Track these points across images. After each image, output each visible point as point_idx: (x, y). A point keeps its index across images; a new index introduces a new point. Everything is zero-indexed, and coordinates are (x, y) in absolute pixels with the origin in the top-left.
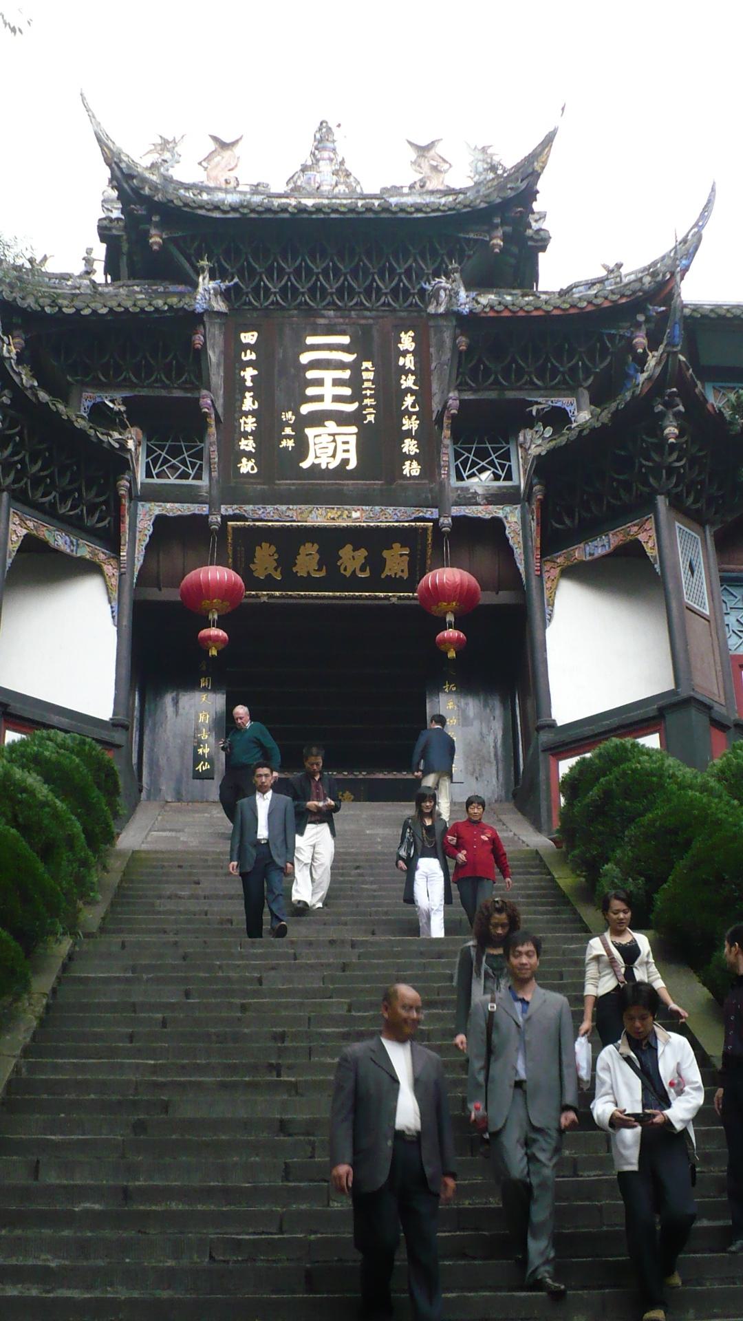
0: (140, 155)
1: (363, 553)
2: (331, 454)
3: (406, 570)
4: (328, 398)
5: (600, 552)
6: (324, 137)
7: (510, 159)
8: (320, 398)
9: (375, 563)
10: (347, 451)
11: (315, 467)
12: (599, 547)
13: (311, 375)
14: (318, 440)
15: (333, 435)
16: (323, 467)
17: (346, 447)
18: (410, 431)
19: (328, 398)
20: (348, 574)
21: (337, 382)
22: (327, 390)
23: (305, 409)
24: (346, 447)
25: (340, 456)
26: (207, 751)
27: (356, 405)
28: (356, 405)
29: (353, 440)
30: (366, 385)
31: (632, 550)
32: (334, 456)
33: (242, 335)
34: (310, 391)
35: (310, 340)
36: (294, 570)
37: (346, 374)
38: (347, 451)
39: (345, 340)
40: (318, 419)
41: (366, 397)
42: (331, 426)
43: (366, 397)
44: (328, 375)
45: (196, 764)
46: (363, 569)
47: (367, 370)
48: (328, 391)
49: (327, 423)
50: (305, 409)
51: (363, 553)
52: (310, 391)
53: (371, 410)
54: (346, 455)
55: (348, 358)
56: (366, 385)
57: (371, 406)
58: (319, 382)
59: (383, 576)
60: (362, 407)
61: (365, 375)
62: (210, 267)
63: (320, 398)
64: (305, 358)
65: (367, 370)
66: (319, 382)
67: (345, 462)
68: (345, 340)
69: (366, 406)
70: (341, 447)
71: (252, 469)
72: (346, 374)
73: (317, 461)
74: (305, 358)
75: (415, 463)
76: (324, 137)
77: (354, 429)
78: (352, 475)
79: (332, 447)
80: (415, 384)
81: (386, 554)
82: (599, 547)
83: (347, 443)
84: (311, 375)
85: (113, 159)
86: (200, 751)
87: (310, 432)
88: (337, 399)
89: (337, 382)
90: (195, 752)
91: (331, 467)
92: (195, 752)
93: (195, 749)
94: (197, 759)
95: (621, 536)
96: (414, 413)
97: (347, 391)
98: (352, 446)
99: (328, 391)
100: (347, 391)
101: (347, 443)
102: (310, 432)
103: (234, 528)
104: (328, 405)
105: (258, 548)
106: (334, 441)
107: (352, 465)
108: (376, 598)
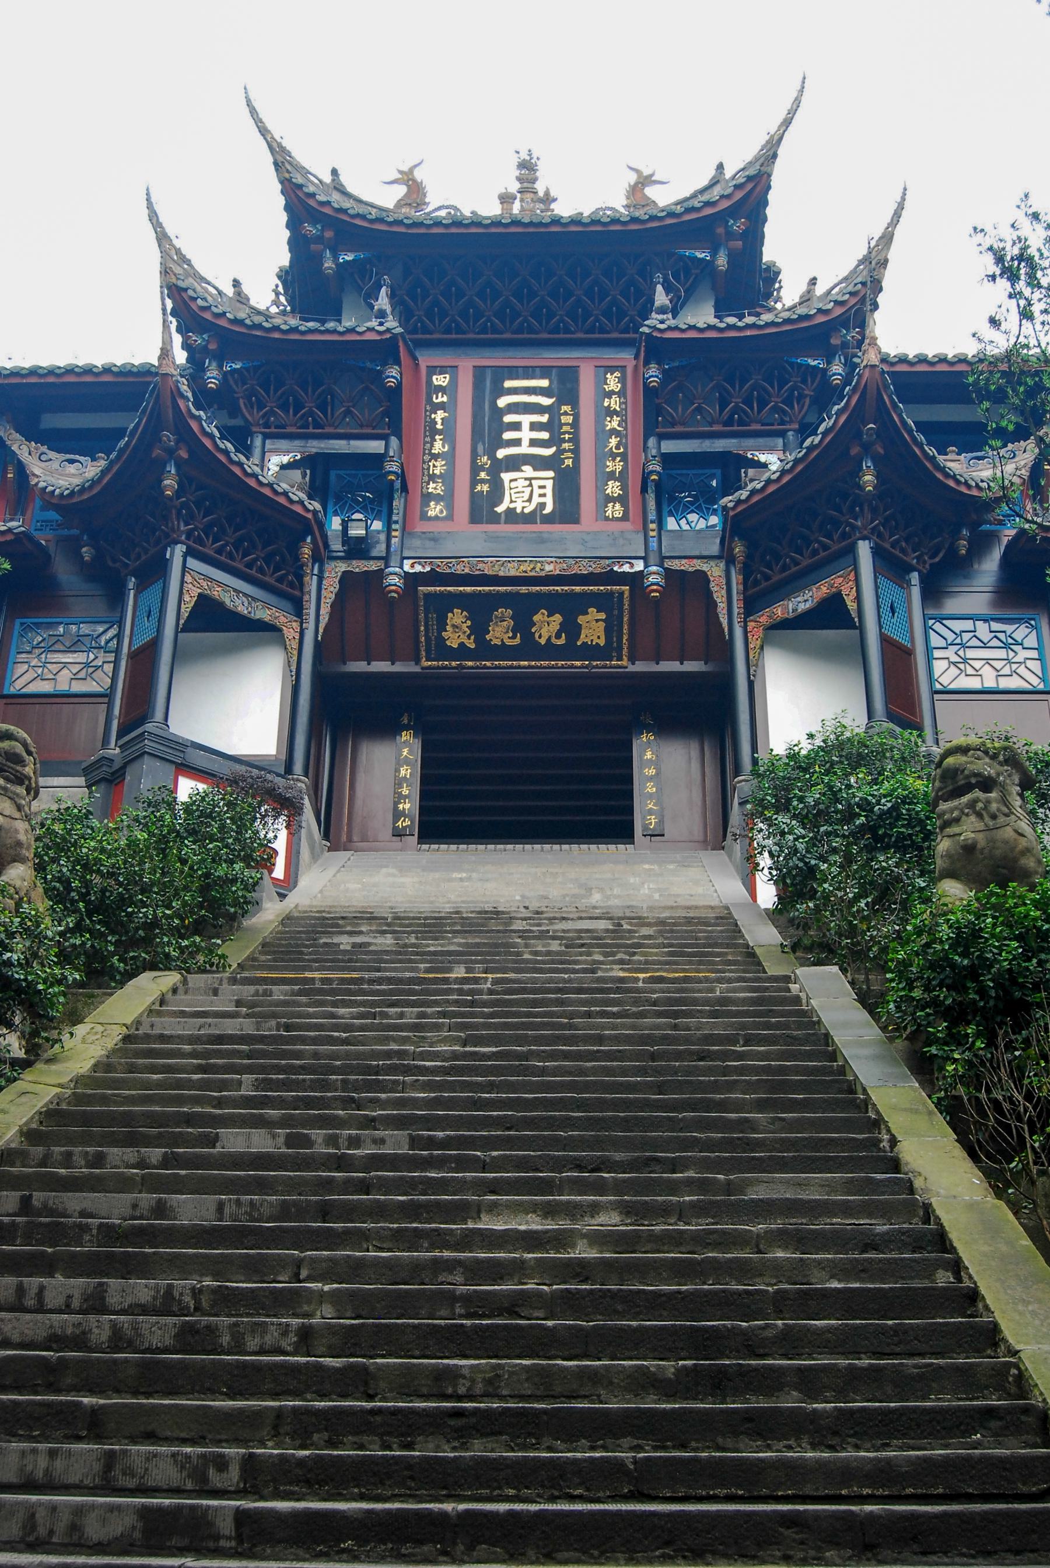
0: (316, 164)
1: (558, 618)
2: (526, 497)
3: (603, 638)
4: (525, 442)
5: (802, 607)
6: (528, 168)
7: (737, 160)
8: (517, 442)
9: (571, 629)
10: (544, 495)
11: (510, 512)
12: (802, 602)
13: (508, 418)
14: (513, 485)
15: (530, 479)
16: (519, 511)
17: (542, 491)
18: (613, 472)
19: (525, 442)
20: (543, 641)
21: (534, 427)
22: (525, 435)
23: (501, 453)
24: (542, 491)
25: (536, 500)
26: (407, 806)
27: (554, 449)
28: (554, 449)
29: (549, 484)
30: (565, 428)
31: (835, 601)
32: (530, 500)
33: (434, 377)
34: (508, 435)
35: (508, 384)
36: (488, 637)
37: (544, 419)
38: (544, 495)
39: (544, 383)
40: (514, 463)
41: (564, 441)
42: (528, 471)
43: (564, 441)
44: (526, 420)
45: (395, 821)
46: (558, 636)
47: (566, 413)
48: (526, 435)
49: (524, 468)
50: (501, 453)
51: (558, 618)
52: (508, 435)
53: (569, 454)
54: (542, 500)
55: (546, 401)
56: (565, 428)
57: (569, 450)
58: (516, 426)
59: (579, 643)
60: (560, 452)
61: (564, 419)
62: (398, 298)
63: (517, 442)
64: (502, 402)
65: (566, 413)
66: (516, 426)
67: (543, 505)
68: (544, 383)
69: (565, 451)
70: (537, 492)
71: (441, 512)
72: (544, 419)
73: (512, 506)
74: (502, 402)
75: (618, 506)
76: (528, 168)
77: (551, 474)
78: (548, 519)
79: (527, 490)
80: (619, 425)
81: (581, 619)
82: (802, 602)
83: (544, 487)
84: (508, 418)
85: (282, 161)
86: (401, 806)
87: (506, 477)
88: (533, 443)
89: (534, 427)
90: (395, 808)
91: (526, 511)
92: (395, 808)
93: (396, 804)
94: (397, 815)
95: (824, 589)
96: (618, 455)
97: (545, 435)
98: (549, 491)
99: (526, 435)
100: (545, 435)
101: (544, 487)
102: (506, 477)
103: (427, 595)
104: (525, 449)
105: (450, 615)
106: (531, 485)
107: (549, 509)
108: (572, 667)
